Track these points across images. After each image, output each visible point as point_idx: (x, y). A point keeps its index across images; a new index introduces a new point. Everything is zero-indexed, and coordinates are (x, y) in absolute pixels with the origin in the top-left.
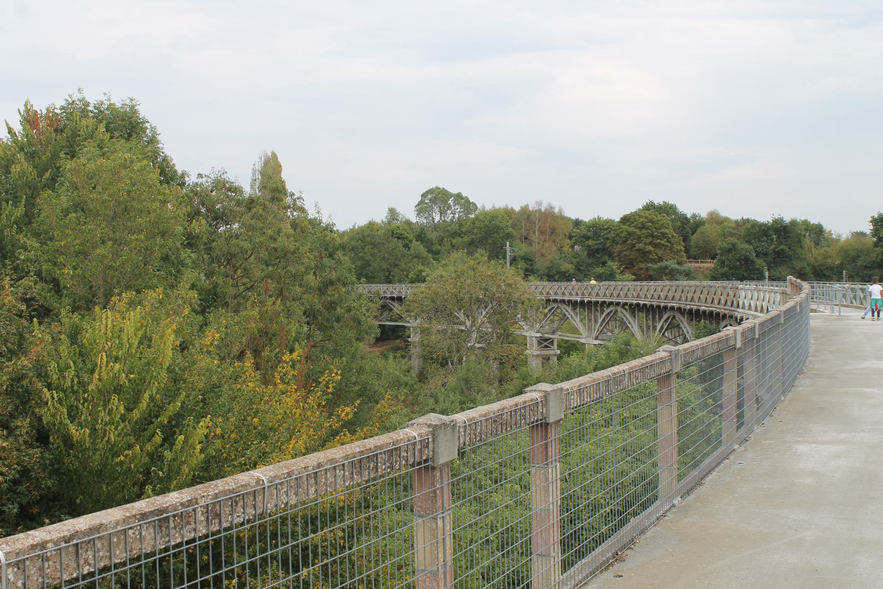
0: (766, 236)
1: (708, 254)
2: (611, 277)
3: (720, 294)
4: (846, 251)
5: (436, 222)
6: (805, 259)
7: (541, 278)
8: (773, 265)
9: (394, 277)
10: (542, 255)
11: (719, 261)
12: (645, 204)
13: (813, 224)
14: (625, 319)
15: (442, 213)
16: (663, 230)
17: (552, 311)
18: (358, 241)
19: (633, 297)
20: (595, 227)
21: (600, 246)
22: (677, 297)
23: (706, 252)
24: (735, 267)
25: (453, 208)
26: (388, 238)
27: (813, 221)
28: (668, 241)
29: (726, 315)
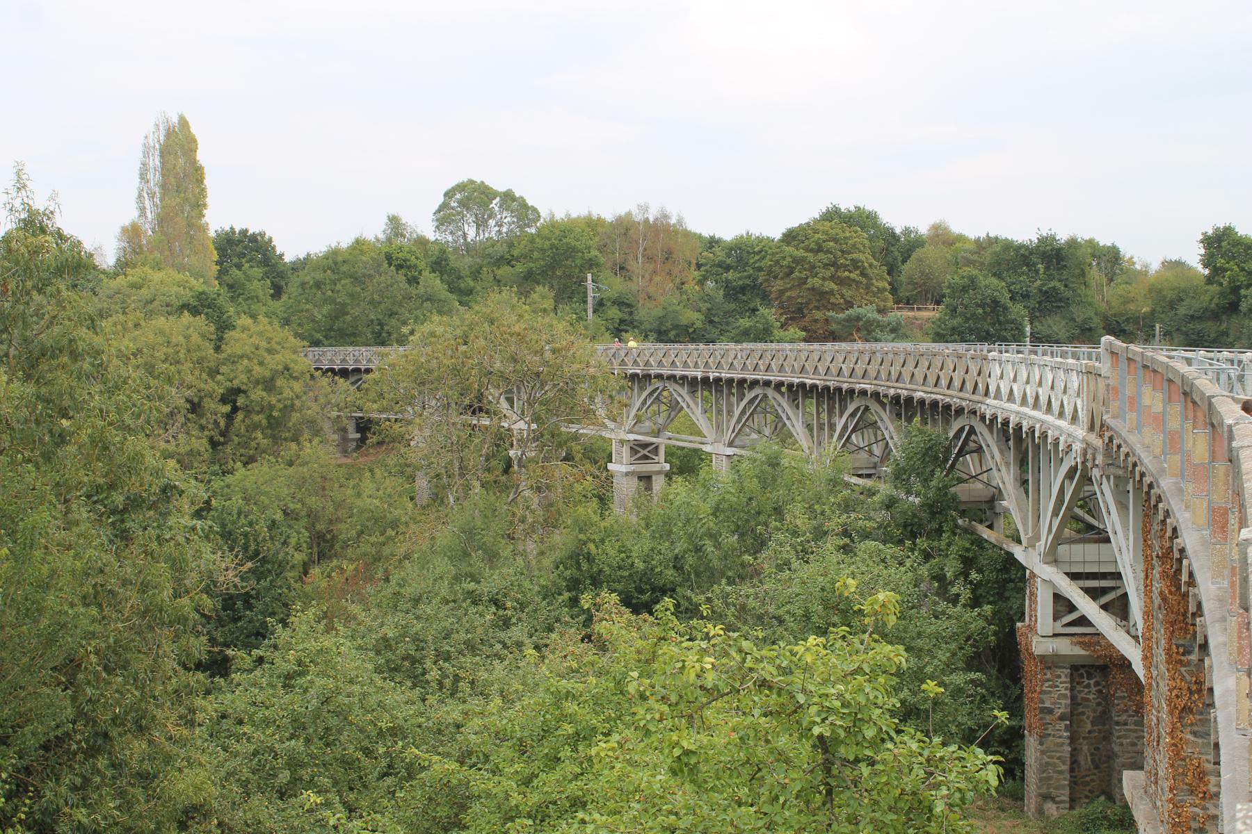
0: (1027, 265)
1: (929, 296)
2: (764, 335)
3: (952, 369)
4: (1160, 292)
5: (469, 240)
6: (1090, 304)
7: (646, 336)
8: (1038, 314)
9: (389, 334)
10: (649, 297)
11: (947, 306)
12: (824, 210)
13: (1104, 247)
14: (780, 412)
15: (481, 224)
16: (855, 256)
17: (655, 395)
18: (325, 272)
19: (793, 371)
20: (740, 249)
21: (747, 282)
22: (872, 373)
23: (927, 293)
24: (974, 317)
25: (499, 216)
26: (380, 265)
27: (1104, 241)
28: (863, 274)
29: (963, 409)
